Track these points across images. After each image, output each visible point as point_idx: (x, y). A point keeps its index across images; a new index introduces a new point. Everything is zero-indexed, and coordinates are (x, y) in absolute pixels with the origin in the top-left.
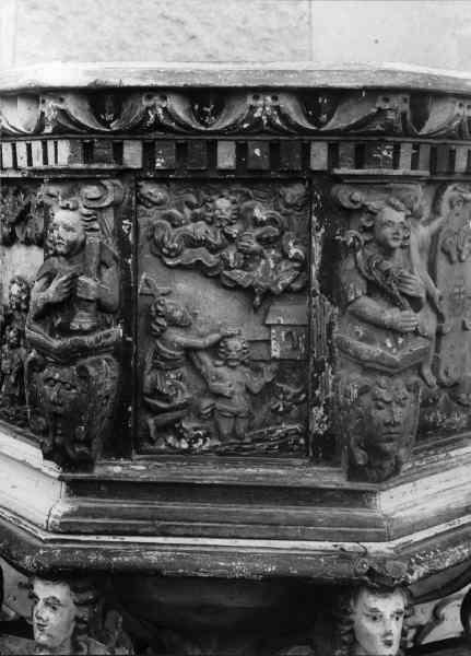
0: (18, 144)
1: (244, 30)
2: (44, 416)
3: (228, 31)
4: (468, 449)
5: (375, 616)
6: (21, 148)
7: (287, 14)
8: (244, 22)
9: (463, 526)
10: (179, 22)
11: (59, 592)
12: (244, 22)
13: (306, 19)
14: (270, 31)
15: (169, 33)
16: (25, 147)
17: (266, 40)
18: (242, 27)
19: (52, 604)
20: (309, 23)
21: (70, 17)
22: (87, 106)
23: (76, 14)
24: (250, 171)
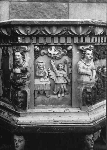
0: (102, 38)
1: (55, 15)
2: (61, 87)
3: (52, 15)
4: (105, 102)
5: (89, 140)
6: (99, 39)
7: (64, 11)
8: (55, 13)
9: (105, 118)
10: (43, 13)
11: (22, 138)
12: (55, 13)
13: (68, 13)
14: (61, 15)
15: (40, 15)
16: (97, 38)
17: (60, 16)
18: (55, 14)
19: (19, 141)
20: (68, 13)
21: (20, 11)
22: (24, 32)
23: (21, 11)
24: (61, 43)
